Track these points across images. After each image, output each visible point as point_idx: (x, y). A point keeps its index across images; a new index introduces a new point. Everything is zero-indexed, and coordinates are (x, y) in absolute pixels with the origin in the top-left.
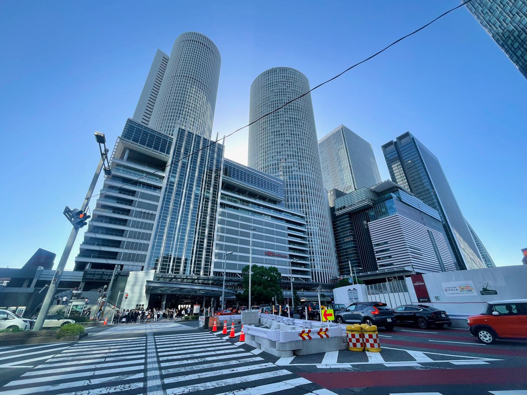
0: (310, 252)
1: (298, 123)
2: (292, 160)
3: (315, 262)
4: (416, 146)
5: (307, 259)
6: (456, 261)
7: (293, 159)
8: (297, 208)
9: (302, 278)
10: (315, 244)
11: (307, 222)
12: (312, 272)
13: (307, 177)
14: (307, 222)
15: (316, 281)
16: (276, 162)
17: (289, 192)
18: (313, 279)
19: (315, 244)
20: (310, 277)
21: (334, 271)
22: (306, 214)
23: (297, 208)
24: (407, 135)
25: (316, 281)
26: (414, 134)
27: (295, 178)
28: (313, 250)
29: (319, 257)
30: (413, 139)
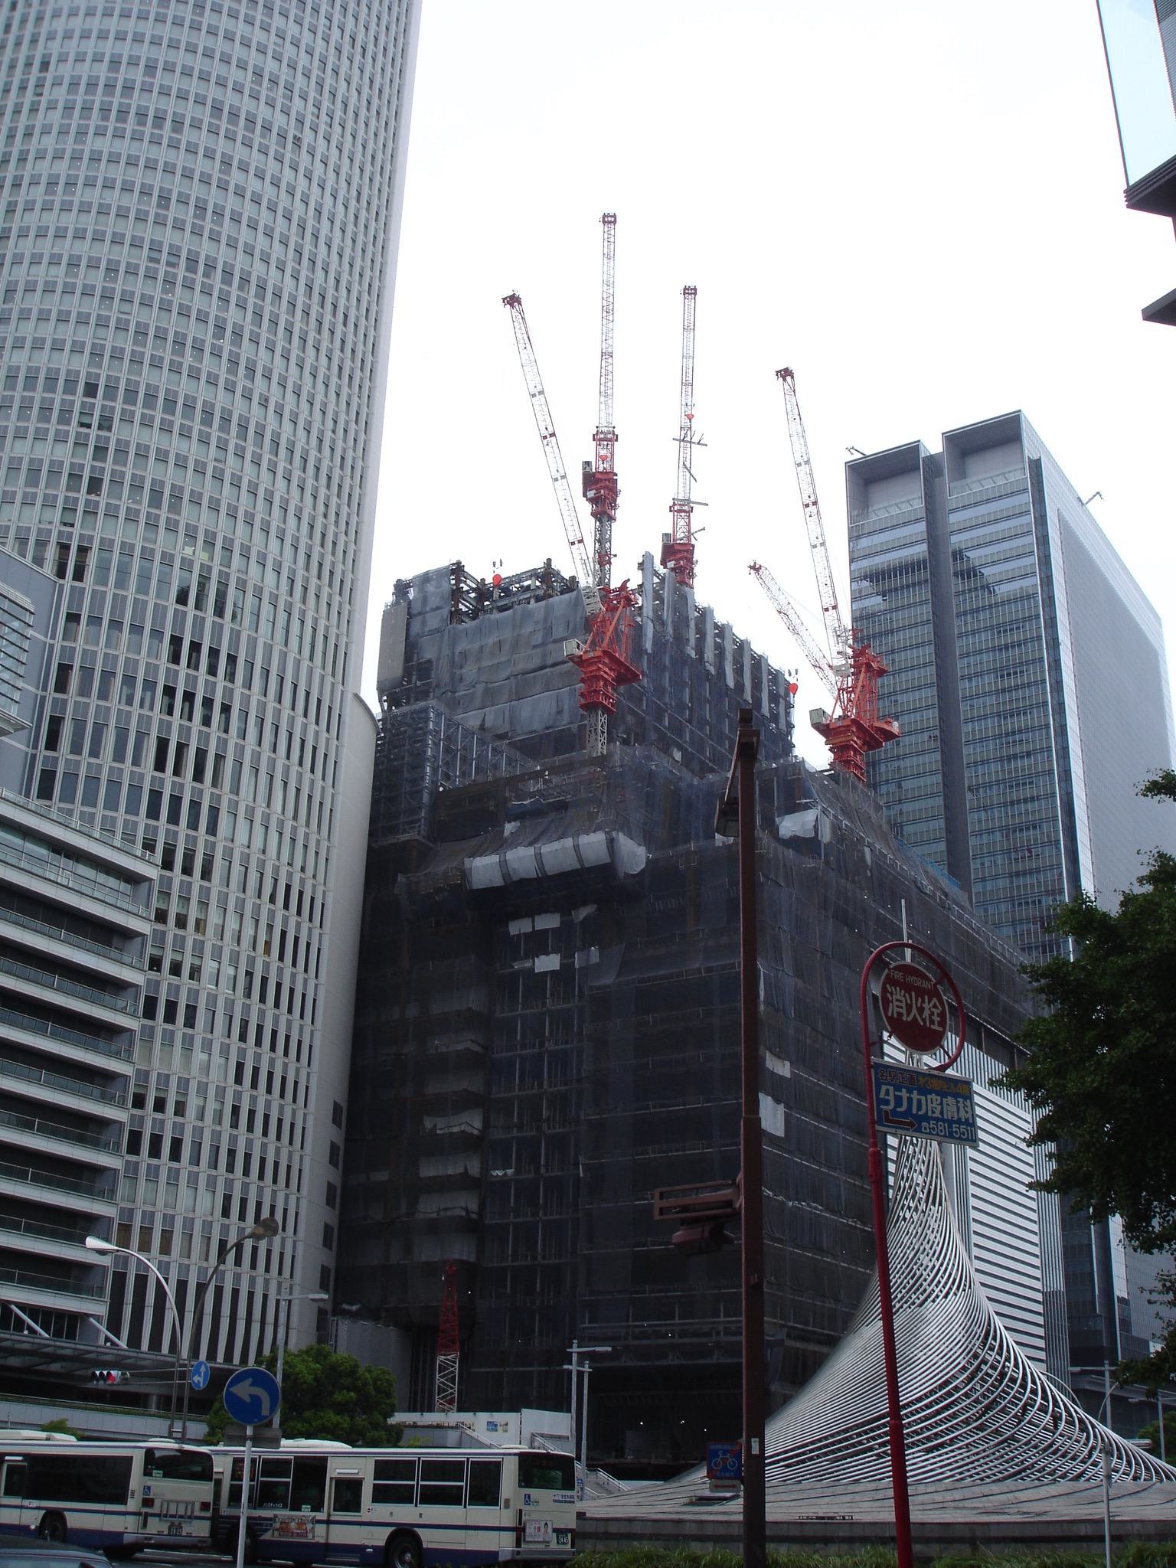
0: (135, 1138)
1: (246, 349)
2: (221, 146)
3: (206, 984)
4: (1042, 520)
5: (107, 1136)
6: (1059, 1284)
7: (167, 428)
8: (112, 804)
9: (33, 1311)
10: (217, 955)
11: (161, 916)
12: (120, 1278)
13: (242, 586)
14: (161, 916)
15: (135, 1340)
16: (102, 71)
17: (75, 677)
18: (114, 1326)
19: (217, 955)
20: (96, 1308)
21: (283, 1298)
22: (167, 864)
23: (112, 804)
24: (1001, 435)
25: (135, 1340)
26: (1050, 434)
27: (145, 577)
28: (194, 994)
29: (225, 1050)
30: (1036, 466)
